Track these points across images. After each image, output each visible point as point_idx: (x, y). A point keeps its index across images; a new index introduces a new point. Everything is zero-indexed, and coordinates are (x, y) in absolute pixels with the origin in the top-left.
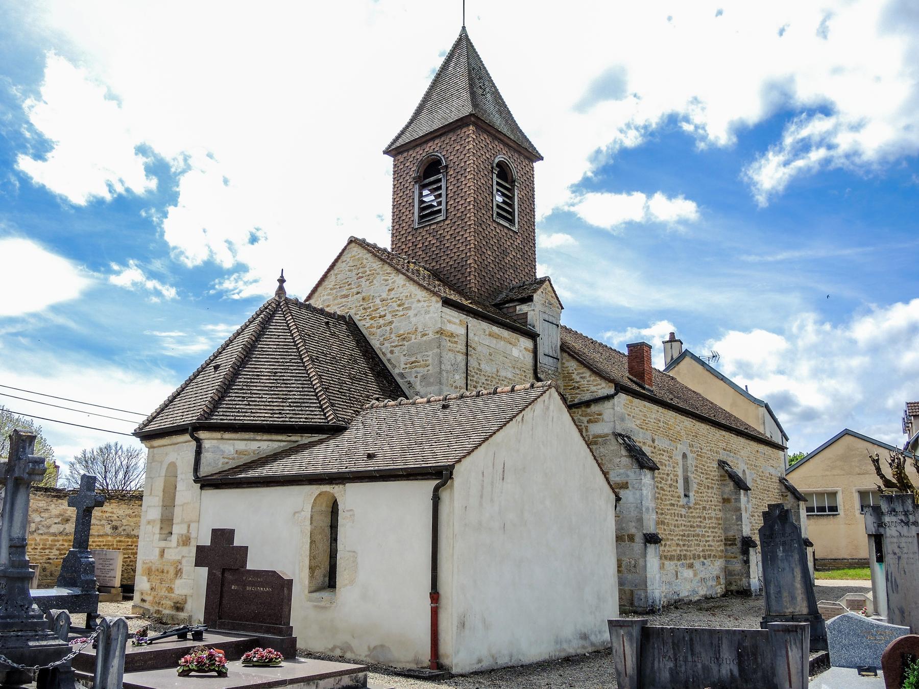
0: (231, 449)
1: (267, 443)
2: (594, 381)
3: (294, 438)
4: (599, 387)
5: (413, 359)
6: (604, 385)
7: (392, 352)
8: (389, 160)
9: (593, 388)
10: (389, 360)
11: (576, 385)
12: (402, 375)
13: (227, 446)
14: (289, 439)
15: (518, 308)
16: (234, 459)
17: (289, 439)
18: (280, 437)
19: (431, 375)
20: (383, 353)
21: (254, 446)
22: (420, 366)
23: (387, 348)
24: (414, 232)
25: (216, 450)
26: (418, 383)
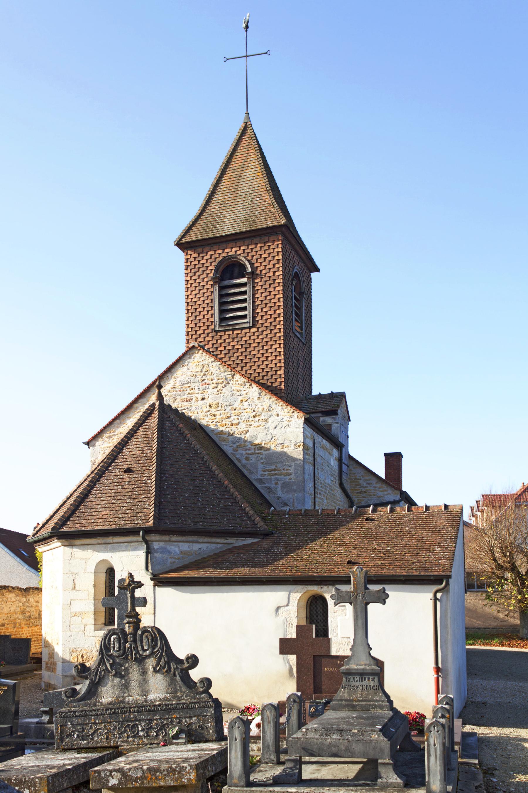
0: (177, 549)
1: (206, 545)
2: (380, 487)
3: (230, 541)
4: (385, 493)
5: (273, 467)
6: (390, 491)
7: (247, 459)
8: (180, 255)
9: (381, 494)
10: (245, 466)
11: (363, 490)
12: (261, 481)
13: (173, 547)
14: (226, 541)
15: (321, 419)
16: (179, 559)
17: (226, 541)
18: (218, 540)
19: (294, 482)
20: (237, 459)
21: (196, 547)
22: (281, 474)
23: (242, 454)
24: (214, 334)
25: (164, 550)
26: (279, 489)
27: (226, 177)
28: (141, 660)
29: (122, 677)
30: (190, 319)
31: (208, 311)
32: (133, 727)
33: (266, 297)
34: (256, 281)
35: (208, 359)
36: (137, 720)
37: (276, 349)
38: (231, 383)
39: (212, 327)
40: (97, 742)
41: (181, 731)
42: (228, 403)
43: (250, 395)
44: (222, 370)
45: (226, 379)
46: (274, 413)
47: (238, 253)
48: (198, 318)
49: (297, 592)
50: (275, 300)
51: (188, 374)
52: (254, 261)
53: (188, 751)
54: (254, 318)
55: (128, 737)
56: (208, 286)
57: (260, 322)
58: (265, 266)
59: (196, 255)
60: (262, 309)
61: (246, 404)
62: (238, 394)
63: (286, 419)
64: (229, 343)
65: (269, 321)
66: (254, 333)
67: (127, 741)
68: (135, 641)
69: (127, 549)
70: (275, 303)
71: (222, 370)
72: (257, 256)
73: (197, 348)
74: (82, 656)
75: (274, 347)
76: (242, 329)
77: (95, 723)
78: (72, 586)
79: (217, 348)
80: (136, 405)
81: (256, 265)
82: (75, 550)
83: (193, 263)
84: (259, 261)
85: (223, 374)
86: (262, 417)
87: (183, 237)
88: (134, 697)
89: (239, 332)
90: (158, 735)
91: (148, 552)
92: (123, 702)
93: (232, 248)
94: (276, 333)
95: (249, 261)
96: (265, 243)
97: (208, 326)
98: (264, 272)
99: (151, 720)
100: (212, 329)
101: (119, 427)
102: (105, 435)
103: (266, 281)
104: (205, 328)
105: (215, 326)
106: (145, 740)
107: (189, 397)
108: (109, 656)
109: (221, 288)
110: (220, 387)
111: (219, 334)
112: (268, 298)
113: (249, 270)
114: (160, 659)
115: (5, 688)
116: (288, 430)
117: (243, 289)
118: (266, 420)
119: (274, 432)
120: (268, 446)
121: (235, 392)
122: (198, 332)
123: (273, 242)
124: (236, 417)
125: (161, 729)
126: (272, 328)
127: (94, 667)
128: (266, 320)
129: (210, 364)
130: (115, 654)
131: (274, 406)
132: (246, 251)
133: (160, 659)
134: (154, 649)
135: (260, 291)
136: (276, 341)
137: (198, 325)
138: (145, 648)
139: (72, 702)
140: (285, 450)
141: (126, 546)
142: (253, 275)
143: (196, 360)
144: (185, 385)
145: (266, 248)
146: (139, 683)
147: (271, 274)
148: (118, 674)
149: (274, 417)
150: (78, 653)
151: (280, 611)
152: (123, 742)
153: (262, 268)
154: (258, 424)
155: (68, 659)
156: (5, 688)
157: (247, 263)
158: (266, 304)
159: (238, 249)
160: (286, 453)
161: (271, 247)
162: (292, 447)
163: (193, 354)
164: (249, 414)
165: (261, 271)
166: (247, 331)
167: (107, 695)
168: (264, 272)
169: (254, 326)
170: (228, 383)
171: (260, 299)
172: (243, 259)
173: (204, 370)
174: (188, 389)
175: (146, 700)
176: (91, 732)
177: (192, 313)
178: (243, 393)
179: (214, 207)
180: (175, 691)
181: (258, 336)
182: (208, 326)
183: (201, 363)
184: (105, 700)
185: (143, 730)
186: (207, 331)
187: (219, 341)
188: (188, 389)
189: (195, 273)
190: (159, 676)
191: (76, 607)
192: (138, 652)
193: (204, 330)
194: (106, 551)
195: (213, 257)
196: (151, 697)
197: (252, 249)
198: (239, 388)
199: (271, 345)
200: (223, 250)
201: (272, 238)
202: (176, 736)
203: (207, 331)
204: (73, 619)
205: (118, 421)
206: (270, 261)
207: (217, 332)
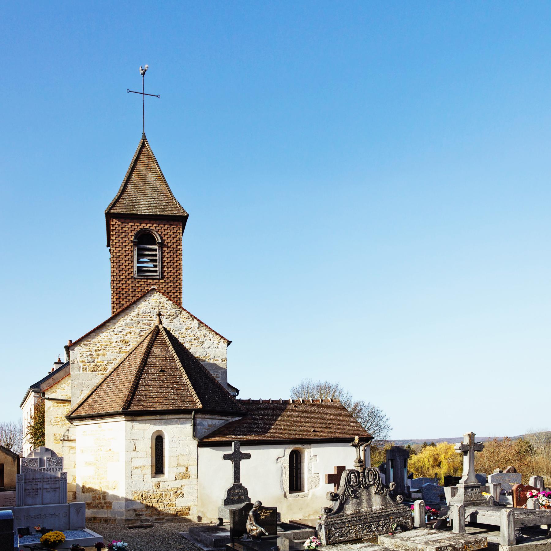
27: (134, 174)
28: (367, 488)
29: (357, 498)
30: (116, 267)
31: (129, 264)
32: (369, 526)
33: (171, 261)
34: (164, 249)
35: (164, 299)
36: (371, 522)
37: (177, 296)
38: (179, 316)
39: (132, 275)
40: (350, 537)
41: (398, 525)
42: (177, 329)
43: (192, 325)
44: (174, 307)
45: (176, 313)
46: (208, 338)
47: (152, 228)
48: (121, 267)
49: (289, 448)
50: (177, 264)
51: (149, 306)
52: (163, 235)
53: (424, 535)
54: (162, 273)
55: (367, 532)
56: (129, 247)
57: (166, 276)
58: (171, 240)
59: (120, 223)
60: (168, 268)
61: (189, 331)
62: (184, 324)
63: (216, 343)
64: (144, 287)
65: (172, 277)
66: (162, 283)
67: (367, 535)
68: (364, 477)
69: (177, 423)
70: (177, 266)
71: (174, 307)
72: (165, 233)
73: (156, 290)
74: (142, 496)
75: (176, 294)
76: (153, 279)
77: (348, 526)
78: (133, 448)
79: (135, 290)
80: (108, 324)
81: (164, 239)
82: (135, 424)
83: (117, 228)
84: (166, 236)
85: (174, 310)
86: (200, 340)
87: (111, 209)
88: (364, 509)
89: (151, 281)
90: (383, 529)
91: (195, 426)
92: (359, 512)
93: (147, 224)
94: (177, 286)
95: (159, 235)
96: (171, 225)
97: (129, 274)
98: (169, 244)
99: (379, 521)
100: (132, 277)
101: (94, 338)
102: (82, 343)
103: (171, 251)
104: (126, 274)
105: (134, 275)
106: (376, 533)
107: (149, 322)
108: (350, 486)
109: (139, 250)
110: (171, 318)
111: (137, 280)
112: (172, 261)
113: (160, 241)
114: (378, 486)
115: (271, 511)
116: (217, 350)
117: (154, 253)
118: (203, 342)
119: (208, 350)
120: (204, 359)
121: (182, 322)
122: (121, 277)
123: (177, 226)
124: (182, 339)
125: (384, 526)
126: (175, 282)
127: (341, 493)
128: (171, 276)
129: (165, 302)
130: (354, 485)
131: (208, 334)
132: (157, 228)
133: (378, 486)
134: (375, 480)
135: (166, 256)
136: (177, 291)
137: (121, 272)
138: (370, 480)
139: (330, 515)
140: (215, 362)
141: (176, 421)
142: (162, 245)
143: (155, 298)
144: (146, 314)
145: (171, 228)
146: (367, 500)
147: (175, 246)
148: (356, 497)
149: (208, 341)
150: (138, 494)
151: (279, 460)
152: (365, 535)
153: (169, 241)
154: (198, 344)
155: (130, 498)
156: (271, 511)
157: (158, 236)
158: (171, 266)
159: (151, 225)
160: (216, 364)
161: (175, 229)
162: (220, 361)
163: (153, 294)
164: (191, 338)
165: (168, 243)
166: (157, 281)
167: (349, 509)
168: (169, 244)
169: (162, 279)
170: (177, 316)
171: (166, 261)
172: (155, 233)
173: (161, 305)
174: (149, 317)
175: (371, 511)
176: (346, 532)
177: (116, 263)
178: (187, 323)
179: (129, 192)
180: (386, 504)
181: (165, 285)
182: (129, 274)
183: (159, 301)
184: (349, 512)
185: (375, 528)
186: (128, 277)
187: (137, 285)
188: (149, 317)
189: (119, 235)
190: (378, 496)
191: (136, 463)
192: (366, 483)
193: (126, 276)
194: (160, 424)
195: (133, 227)
196: (374, 508)
197: (162, 227)
198: (185, 320)
199: (174, 293)
200: (141, 224)
201: (175, 223)
202: (396, 529)
203: (128, 277)
204: (134, 471)
205: (94, 334)
206: (174, 238)
207: (135, 279)
